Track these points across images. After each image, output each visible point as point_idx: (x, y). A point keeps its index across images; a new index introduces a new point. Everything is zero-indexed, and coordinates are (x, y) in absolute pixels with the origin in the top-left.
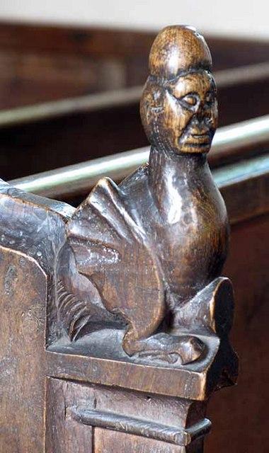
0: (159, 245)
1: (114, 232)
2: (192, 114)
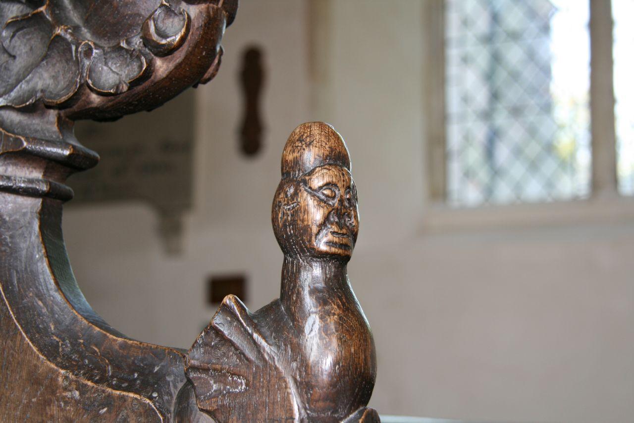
0: (294, 365)
1: (241, 354)
2: (330, 209)
